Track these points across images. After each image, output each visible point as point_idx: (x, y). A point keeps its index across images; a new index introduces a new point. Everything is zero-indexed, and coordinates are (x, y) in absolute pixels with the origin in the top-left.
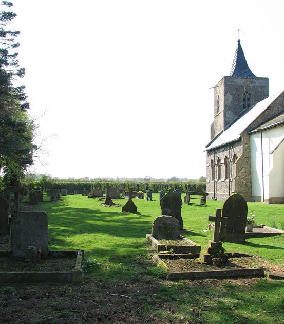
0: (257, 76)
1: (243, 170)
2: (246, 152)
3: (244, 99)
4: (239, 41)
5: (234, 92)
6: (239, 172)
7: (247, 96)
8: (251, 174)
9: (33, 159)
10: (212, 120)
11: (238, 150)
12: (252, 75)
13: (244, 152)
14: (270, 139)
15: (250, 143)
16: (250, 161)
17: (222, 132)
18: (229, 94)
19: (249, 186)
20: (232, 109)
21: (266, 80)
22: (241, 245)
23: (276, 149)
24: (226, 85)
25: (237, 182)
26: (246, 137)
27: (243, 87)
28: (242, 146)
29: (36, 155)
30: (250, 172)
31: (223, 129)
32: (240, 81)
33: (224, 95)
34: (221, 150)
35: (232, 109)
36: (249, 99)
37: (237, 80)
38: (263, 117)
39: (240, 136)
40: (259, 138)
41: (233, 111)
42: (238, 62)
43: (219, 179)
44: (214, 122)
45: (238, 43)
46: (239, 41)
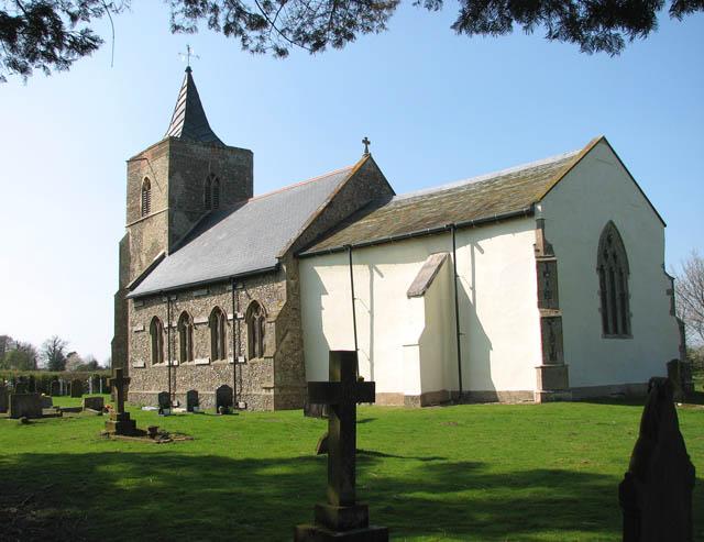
0: (228, 142)
1: (288, 337)
2: (292, 297)
3: (208, 189)
4: (189, 70)
5: (188, 172)
6: (282, 340)
7: (213, 184)
8: (302, 346)
9: (130, 374)
10: (121, 232)
11: (273, 297)
12: (215, 142)
13: (288, 297)
14: (372, 267)
15: (298, 276)
16: (300, 317)
17: (163, 257)
18: (178, 176)
19: (300, 372)
20: (185, 208)
21: (248, 154)
22: (77, 452)
23: (428, 286)
24: (172, 157)
25: (277, 363)
26: (292, 262)
27: (206, 163)
28: (285, 282)
29: (674, 358)
30: (301, 341)
31: (165, 250)
32: (199, 150)
33: (170, 177)
34: (195, 294)
35: (185, 208)
36: (216, 190)
37: (195, 148)
38: (320, 222)
39: (277, 261)
40: (344, 267)
41: (186, 213)
42: (188, 110)
43: (187, 355)
44: (128, 235)
45: (186, 74)
46: (189, 70)
